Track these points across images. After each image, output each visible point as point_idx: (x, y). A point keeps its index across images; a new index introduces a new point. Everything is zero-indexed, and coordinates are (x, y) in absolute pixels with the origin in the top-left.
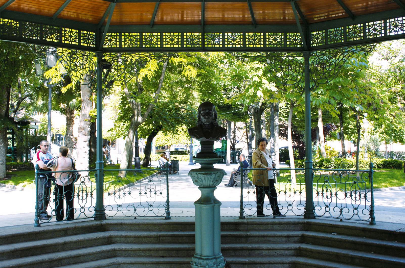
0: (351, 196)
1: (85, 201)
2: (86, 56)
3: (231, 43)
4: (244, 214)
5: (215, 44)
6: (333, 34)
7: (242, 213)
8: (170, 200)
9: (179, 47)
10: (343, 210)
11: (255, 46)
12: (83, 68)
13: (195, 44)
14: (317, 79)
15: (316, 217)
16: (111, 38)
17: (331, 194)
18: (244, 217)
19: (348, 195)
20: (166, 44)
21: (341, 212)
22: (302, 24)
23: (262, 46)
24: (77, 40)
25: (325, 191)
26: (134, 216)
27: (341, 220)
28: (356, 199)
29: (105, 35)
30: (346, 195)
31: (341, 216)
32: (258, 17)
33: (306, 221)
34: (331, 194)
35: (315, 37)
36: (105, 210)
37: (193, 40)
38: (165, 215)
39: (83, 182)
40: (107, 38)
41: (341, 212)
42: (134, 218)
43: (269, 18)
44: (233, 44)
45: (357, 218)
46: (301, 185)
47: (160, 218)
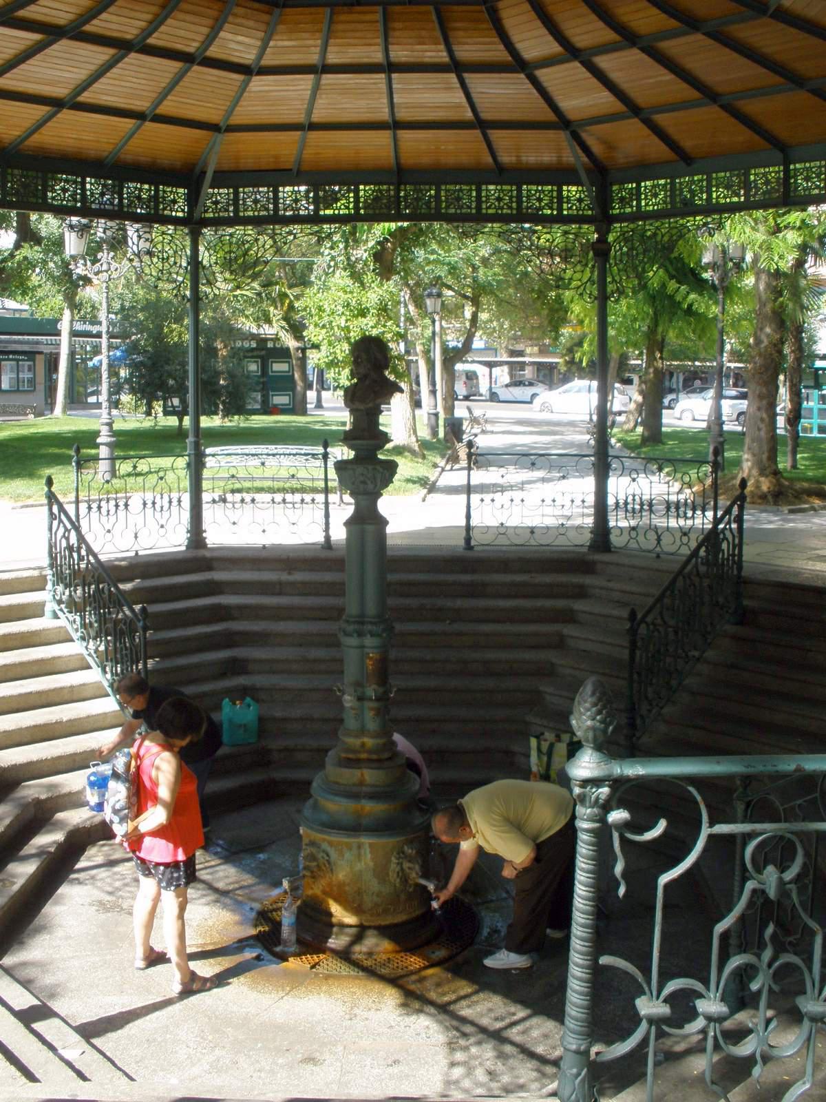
0: (99, 507)
1: (112, 519)
2: (170, 235)
4: (473, 543)
6: (534, 195)
8: (473, 523)
9: (471, 213)
11: (728, 200)
12: (163, 259)
14: (580, 280)
17: (170, 502)
22: (588, 171)
23: (514, 212)
24: (352, 195)
25: (158, 496)
26: (134, 549)
27: (658, 556)
32: (506, 158)
34: (170, 502)
35: (534, 195)
37: (459, 199)
39: (161, 478)
43: (531, 158)
46: (469, 489)
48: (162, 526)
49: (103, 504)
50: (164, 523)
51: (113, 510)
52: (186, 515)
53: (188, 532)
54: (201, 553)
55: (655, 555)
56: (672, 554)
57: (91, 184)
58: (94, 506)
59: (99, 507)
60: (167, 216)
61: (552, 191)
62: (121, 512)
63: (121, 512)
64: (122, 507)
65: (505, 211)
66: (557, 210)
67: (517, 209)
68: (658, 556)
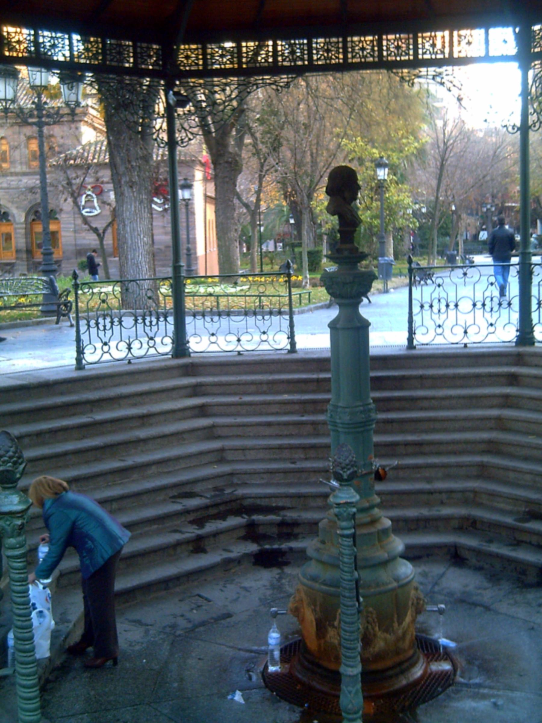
0: (97, 324)
3: (288, 59)
4: (415, 342)
5: (366, 56)
7: (410, 339)
10: (132, 346)
13: (331, 59)
15: (192, 355)
16: (330, 47)
18: (415, 348)
19: (140, 321)
20: (353, 57)
21: (129, 348)
27: (130, 362)
28: (105, 329)
29: (178, 49)
30: (136, 321)
31: (130, 355)
33: (521, 349)
36: (188, 342)
38: (289, 347)
40: (182, 54)
41: (129, 348)
42: (463, 345)
44: (325, 59)
45: (109, 358)
47: (479, 345)
48: (491, 325)
49: (101, 321)
50: (493, 323)
51: (108, 326)
52: (515, 316)
53: (517, 331)
54: (414, 352)
55: (127, 362)
56: (95, 363)
57: (282, 45)
58: (93, 323)
59: (97, 324)
60: (392, 61)
61: (338, 42)
62: (116, 328)
63: (116, 328)
64: (116, 323)
65: (227, 66)
66: (308, 61)
67: (343, 59)
68: (130, 362)
